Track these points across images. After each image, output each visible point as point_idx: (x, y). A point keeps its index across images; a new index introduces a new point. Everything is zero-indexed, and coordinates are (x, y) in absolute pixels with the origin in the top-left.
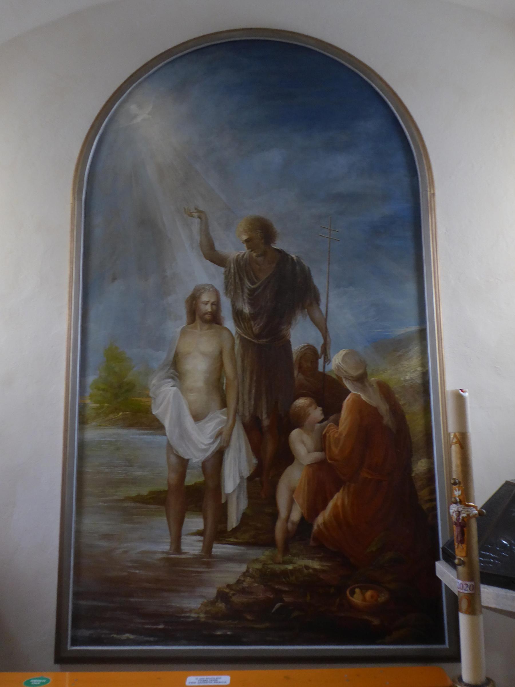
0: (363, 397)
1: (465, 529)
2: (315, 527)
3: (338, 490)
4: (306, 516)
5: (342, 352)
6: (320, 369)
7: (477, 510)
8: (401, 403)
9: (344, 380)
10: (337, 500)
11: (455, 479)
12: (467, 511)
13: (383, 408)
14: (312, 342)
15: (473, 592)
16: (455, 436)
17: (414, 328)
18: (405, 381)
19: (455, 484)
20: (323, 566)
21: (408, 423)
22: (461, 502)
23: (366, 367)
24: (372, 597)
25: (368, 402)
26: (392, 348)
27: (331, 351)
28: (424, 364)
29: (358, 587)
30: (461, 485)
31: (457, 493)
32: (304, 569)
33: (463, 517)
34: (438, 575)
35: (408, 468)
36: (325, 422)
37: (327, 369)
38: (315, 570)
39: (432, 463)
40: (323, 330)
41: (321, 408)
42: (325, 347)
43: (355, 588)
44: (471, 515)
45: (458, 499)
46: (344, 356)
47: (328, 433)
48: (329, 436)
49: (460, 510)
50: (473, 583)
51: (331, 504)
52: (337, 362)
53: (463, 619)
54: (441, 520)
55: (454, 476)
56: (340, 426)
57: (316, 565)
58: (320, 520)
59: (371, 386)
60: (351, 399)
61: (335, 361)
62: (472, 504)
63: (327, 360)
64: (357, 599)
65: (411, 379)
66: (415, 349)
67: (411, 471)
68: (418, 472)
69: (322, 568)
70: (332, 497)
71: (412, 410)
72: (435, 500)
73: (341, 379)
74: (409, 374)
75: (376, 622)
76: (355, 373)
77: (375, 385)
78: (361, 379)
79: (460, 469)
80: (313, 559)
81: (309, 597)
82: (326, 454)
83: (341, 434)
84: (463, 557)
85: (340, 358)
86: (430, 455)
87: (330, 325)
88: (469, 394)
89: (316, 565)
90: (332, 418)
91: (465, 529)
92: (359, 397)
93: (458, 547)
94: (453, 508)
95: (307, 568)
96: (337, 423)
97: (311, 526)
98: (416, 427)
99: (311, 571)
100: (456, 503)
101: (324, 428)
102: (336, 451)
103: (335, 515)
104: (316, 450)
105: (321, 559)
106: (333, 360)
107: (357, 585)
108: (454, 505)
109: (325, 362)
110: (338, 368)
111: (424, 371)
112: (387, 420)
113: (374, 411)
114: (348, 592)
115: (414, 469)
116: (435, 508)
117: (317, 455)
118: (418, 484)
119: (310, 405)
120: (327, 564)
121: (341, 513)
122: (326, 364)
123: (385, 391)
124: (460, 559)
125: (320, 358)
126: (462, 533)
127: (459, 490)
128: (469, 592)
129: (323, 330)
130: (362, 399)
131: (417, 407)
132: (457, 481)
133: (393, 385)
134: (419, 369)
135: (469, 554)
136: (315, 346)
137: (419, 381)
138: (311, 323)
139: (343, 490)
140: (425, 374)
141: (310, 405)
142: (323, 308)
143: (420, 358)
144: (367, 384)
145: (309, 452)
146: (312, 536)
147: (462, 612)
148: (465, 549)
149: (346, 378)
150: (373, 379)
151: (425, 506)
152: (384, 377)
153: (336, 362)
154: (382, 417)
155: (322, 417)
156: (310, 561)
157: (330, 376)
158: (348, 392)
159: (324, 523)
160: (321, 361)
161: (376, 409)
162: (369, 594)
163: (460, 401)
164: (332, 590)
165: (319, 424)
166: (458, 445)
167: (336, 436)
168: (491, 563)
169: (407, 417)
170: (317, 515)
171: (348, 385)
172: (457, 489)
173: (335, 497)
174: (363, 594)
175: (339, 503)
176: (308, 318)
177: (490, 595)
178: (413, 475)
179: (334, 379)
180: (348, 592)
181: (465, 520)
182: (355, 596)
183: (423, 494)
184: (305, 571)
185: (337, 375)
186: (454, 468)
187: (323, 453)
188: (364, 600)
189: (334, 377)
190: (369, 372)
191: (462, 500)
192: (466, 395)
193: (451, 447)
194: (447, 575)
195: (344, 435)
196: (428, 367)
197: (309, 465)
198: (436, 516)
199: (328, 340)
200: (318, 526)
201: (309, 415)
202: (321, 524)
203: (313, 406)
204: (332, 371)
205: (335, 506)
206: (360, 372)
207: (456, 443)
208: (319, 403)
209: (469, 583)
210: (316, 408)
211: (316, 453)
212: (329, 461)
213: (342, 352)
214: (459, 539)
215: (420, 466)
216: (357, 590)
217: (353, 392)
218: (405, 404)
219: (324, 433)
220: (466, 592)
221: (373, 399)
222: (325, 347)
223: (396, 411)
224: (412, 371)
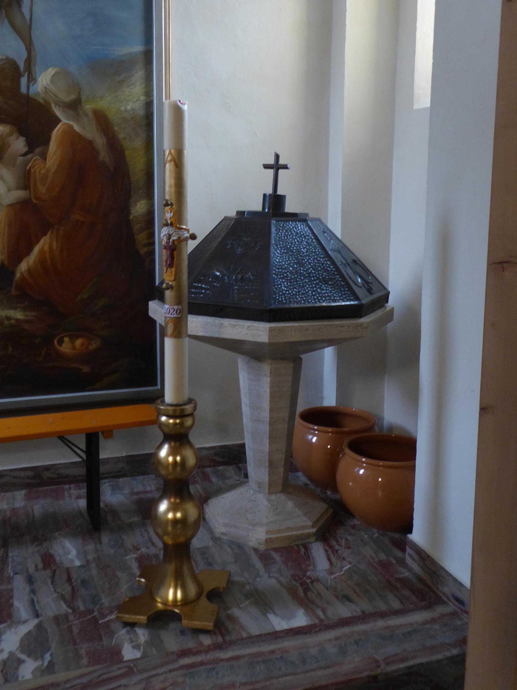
0: (77, 128)
1: (175, 253)
2: (18, 275)
3: (45, 234)
4: (6, 263)
5: (51, 71)
6: (23, 90)
7: (188, 232)
8: (121, 136)
9: (53, 105)
10: (44, 244)
11: (167, 200)
12: (178, 234)
13: (100, 141)
14: (12, 54)
15: (179, 316)
16: (170, 153)
17: (138, 48)
18: (126, 111)
19: (167, 205)
20: (26, 316)
21: (128, 160)
22: (172, 224)
23: (80, 92)
24: (82, 345)
25: (82, 134)
26: (112, 71)
27: (37, 68)
28: (149, 93)
29: (66, 336)
30: (174, 207)
31: (169, 215)
32: (5, 320)
33: (173, 240)
34: (151, 314)
35: (125, 210)
36: (30, 156)
37: (33, 90)
38: (17, 320)
39: (153, 205)
40: (25, 35)
41: (24, 139)
42: (29, 62)
43: (63, 337)
44: (182, 238)
45: (169, 222)
46: (53, 76)
47: (33, 168)
48: (35, 172)
49: (171, 233)
50: (180, 307)
51: (36, 249)
52: (44, 83)
53: (169, 343)
54: (159, 265)
55: (167, 197)
56: (47, 161)
57: (18, 315)
58: (24, 266)
59: (86, 115)
60: (61, 129)
61: (42, 81)
62: (184, 227)
63: (32, 79)
64: (65, 347)
65: (133, 109)
66: (139, 74)
67: (129, 213)
68: (136, 214)
69: (27, 318)
70: (38, 241)
71: (133, 146)
72: (153, 244)
73: (49, 104)
74: (131, 104)
75: (86, 369)
76: (67, 98)
77: (91, 114)
78: (74, 106)
79: (173, 189)
80: (15, 309)
81: (10, 350)
82: (30, 193)
83: (48, 170)
84: (171, 281)
85: (49, 77)
86: (150, 196)
87: (35, 34)
88: (188, 107)
89: (18, 315)
90: (37, 150)
91: (175, 253)
92: (71, 127)
93: (166, 272)
94: (165, 231)
95: (8, 318)
96: (44, 156)
97: (13, 273)
98: (136, 164)
99: (13, 321)
100: (167, 225)
101: (28, 163)
102: (42, 189)
103: (41, 261)
104: (18, 188)
105: (24, 309)
106: (39, 80)
107: (66, 334)
108: (165, 228)
109: (29, 81)
110: (46, 90)
111: (149, 100)
112: (104, 155)
113: (90, 144)
114: (56, 342)
115: (133, 211)
116: (153, 252)
117: (19, 194)
118: (136, 227)
119: (10, 134)
120: (32, 314)
121: (48, 261)
122: (31, 85)
123: (102, 120)
124: (168, 284)
125: (24, 76)
126: (172, 257)
127: (171, 212)
128: (175, 316)
129: (25, 35)
130: (74, 130)
131: (138, 143)
132: (169, 202)
133: (111, 115)
134: (143, 98)
135: (177, 278)
136: (16, 60)
137: (141, 112)
138: (11, 29)
139: (52, 233)
140: (149, 105)
141: (10, 134)
142: (26, 10)
143: (143, 86)
144: (81, 112)
145: (9, 190)
146: (14, 285)
147: (168, 336)
148: (174, 273)
149: (56, 104)
150: (88, 107)
151: (143, 251)
152: (102, 104)
153: (44, 82)
154: (97, 153)
155: (26, 149)
156: (12, 311)
157: (34, 100)
158: (59, 121)
159: (29, 270)
160: (24, 80)
161: (91, 143)
162: (78, 342)
163: (178, 113)
164: (38, 341)
165: (22, 158)
166: (173, 163)
167: (43, 172)
168: (202, 293)
169: (127, 153)
170: (20, 261)
171: (58, 112)
172: (169, 211)
173: (42, 241)
174: (73, 342)
175: (46, 248)
176: (6, 21)
177: (197, 324)
178: (131, 217)
179: (39, 103)
180: (56, 342)
181: (176, 243)
182: (64, 345)
183: (141, 237)
184: (7, 322)
185: (44, 99)
186: (167, 189)
187: (28, 191)
188: (74, 348)
189: (41, 101)
190: (84, 98)
191: (174, 222)
192: (185, 108)
193: (165, 166)
194: (159, 311)
195: (52, 171)
196: (153, 96)
197: (10, 205)
198: (153, 261)
199: (33, 53)
200: (22, 273)
201: (9, 146)
202: (25, 271)
203: (15, 136)
204: (38, 93)
205: (42, 251)
206: (73, 97)
207: (171, 161)
208: (22, 132)
209: (176, 307)
210: (18, 138)
211: (18, 191)
212: (34, 201)
213: (51, 71)
214: (168, 264)
215: (139, 208)
216: (66, 339)
217: (64, 120)
218: (124, 139)
219: (28, 168)
220: (173, 316)
221: (89, 131)
222: (29, 62)
223: (115, 146)
224: (135, 100)
